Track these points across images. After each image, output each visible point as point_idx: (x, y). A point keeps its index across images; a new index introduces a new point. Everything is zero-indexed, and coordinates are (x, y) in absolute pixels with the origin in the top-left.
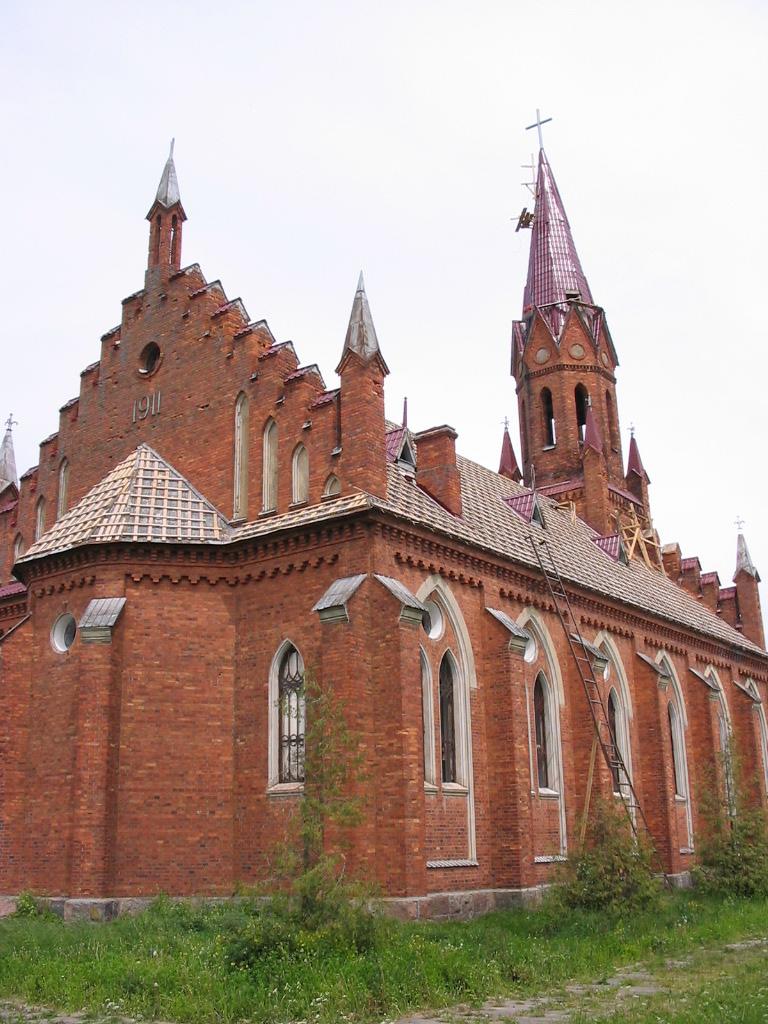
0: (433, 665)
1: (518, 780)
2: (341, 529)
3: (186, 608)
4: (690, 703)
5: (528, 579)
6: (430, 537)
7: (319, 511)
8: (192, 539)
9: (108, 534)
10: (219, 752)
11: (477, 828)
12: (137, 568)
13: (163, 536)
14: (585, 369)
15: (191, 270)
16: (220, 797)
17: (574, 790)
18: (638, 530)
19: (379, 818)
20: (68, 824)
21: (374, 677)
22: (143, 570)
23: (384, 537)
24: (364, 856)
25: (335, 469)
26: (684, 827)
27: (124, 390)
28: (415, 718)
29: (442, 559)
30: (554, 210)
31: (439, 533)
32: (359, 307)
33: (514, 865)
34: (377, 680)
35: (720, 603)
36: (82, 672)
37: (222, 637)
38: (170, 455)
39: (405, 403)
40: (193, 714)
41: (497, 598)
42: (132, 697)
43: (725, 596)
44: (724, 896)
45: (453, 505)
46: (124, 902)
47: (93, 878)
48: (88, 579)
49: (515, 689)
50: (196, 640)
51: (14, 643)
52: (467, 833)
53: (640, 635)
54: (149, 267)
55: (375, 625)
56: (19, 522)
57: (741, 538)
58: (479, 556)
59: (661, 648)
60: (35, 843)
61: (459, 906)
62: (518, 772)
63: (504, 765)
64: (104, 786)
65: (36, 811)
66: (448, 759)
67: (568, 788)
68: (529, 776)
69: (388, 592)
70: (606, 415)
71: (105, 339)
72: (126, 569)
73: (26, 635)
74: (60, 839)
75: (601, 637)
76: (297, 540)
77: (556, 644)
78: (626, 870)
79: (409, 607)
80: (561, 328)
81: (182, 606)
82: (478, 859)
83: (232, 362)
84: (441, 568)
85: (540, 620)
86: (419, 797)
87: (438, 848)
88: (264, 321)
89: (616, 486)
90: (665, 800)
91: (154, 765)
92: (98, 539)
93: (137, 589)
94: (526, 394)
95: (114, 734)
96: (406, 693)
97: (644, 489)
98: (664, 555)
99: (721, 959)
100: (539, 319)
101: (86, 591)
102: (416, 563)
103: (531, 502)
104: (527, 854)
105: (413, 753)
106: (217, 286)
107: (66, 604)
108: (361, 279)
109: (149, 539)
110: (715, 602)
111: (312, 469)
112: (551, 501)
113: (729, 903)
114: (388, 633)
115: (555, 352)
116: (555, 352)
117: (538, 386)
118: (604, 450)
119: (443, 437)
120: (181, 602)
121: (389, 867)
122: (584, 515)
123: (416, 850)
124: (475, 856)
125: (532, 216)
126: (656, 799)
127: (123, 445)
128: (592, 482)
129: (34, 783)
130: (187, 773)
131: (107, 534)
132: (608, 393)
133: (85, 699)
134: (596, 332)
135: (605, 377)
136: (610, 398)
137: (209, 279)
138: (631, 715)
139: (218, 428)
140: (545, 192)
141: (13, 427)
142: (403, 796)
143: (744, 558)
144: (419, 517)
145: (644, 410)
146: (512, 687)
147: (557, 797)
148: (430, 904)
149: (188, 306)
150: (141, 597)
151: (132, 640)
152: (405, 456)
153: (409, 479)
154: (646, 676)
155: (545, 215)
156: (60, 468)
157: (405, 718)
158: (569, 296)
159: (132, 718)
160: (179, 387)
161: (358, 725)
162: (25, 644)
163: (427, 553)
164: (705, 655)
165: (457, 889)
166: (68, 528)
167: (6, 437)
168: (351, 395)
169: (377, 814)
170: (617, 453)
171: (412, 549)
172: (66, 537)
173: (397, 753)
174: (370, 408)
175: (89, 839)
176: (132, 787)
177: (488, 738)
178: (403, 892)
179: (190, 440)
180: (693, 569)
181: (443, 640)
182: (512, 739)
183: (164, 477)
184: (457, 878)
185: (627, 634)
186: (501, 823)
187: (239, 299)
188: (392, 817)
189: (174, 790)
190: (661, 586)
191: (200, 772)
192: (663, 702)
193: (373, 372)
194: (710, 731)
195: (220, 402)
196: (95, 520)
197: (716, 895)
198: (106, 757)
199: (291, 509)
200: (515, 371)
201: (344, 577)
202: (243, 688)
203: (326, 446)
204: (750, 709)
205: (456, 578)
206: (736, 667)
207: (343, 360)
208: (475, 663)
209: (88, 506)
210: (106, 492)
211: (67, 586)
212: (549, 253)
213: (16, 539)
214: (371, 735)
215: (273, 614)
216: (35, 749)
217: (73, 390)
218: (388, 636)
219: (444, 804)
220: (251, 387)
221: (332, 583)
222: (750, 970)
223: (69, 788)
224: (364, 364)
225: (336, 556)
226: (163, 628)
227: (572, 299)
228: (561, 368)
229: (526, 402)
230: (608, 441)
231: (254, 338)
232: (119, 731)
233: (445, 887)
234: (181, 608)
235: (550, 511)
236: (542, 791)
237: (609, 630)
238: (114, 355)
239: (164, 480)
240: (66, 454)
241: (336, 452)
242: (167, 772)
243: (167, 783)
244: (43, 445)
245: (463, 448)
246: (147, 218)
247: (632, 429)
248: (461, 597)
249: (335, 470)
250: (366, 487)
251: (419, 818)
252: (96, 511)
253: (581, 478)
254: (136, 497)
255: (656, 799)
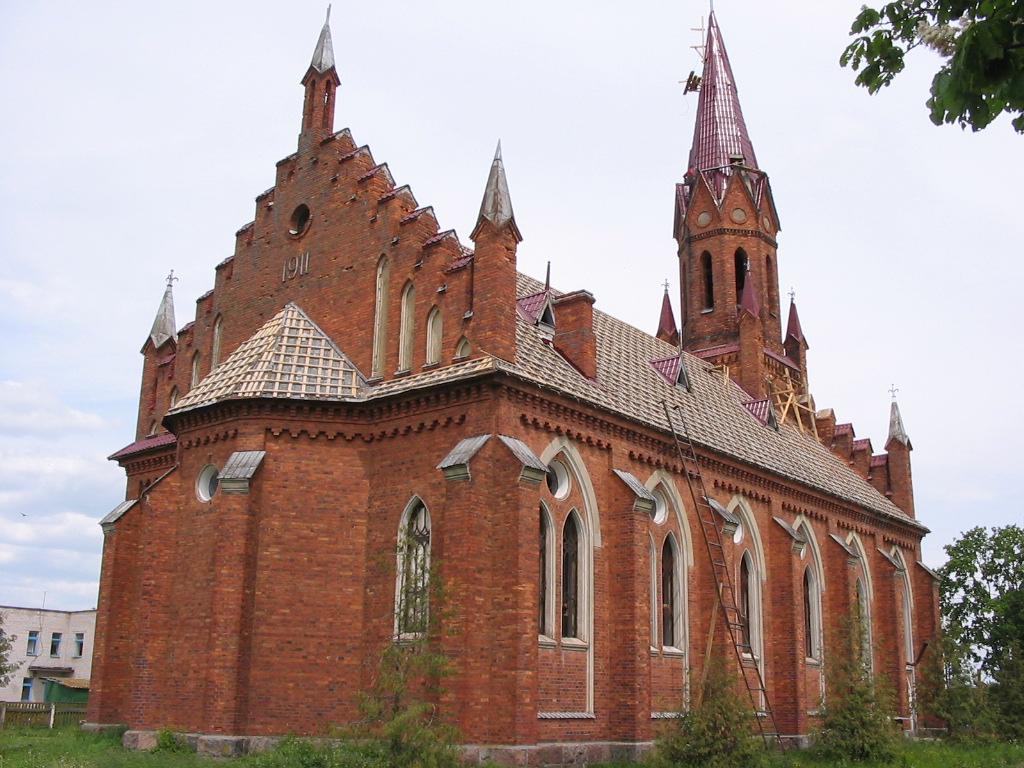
0: (557, 524)
1: (637, 637)
2: (468, 391)
3: (323, 462)
4: (829, 568)
6: (557, 401)
7: (433, 377)
8: (330, 396)
9: (249, 390)
10: (349, 600)
12: (276, 423)
13: (303, 392)
14: (745, 233)
15: (341, 135)
16: (349, 645)
18: (791, 395)
19: (493, 669)
20: (206, 665)
21: (494, 534)
22: (282, 425)
24: (477, 704)
25: (466, 332)
27: (276, 250)
28: (531, 575)
30: (722, 75)
32: (496, 175)
33: (630, 719)
35: (871, 470)
36: (222, 521)
37: (357, 491)
38: (315, 314)
40: (325, 564)
41: (626, 460)
42: (269, 546)
43: (877, 463)
45: (588, 369)
46: (258, 742)
47: (225, 716)
48: (231, 433)
50: (331, 493)
51: (161, 492)
52: (585, 687)
53: (777, 500)
54: (302, 130)
55: (497, 483)
56: (176, 376)
57: (894, 406)
60: (176, 682)
63: (624, 623)
64: (238, 629)
65: (177, 651)
67: (694, 646)
69: (510, 452)
70: (765, 279)
71: (259, 200)
72: (266, 423)
73: (173, 484)
74: (198, 679)
75: (735, 501)
76: (427, 400)
77: (687, 506)
79: (528, 468)
80: (724, 192)
81: (318, 460)
83: (376, 226)
84: (569, 431)
85: (671, 483)
87: (555, 700)
88: (408, 186)
89: (773, 351)
90: (794, 662)
91: (287, 611)
92: (240, 395)
93: (277, 443)
95: (250, 581)
96: (523, 550)
100: (702, 182)
101: (229, 443)
102: (541, 425)
104: (643, 709)
105: (528, 608)
106: (366, 151)
107: (210, 456)
108: (499, 148)
109: (288, 395)
110: (867, 468)
112: (707, 365)
114: (509, 492)
115: (716, 216)
116: (716, 216)
117: (698, 249)
118: (761, 315)
120: (317, 457)
121: (501, 716)
122: (739, 379)
123: (528, 700)
124: (592, 710)
125: (700, 79)
126: (785, 660)
127: (273, 303)
129: (176, 625)
130: (318, 620)
131: (249, 390)
132: (768, 257)
133: (224, 547)
134: (758, 198)
135: (766, 242)
136: (770, 264)
137: (359, 144)
139: (360, 289)
140: (714, 54)
141: (174, 283)
142: (516, 649)
143: (897, 427)
144: (547, 380)
145: (807, 275)
147: (681, 656)
148: (539, 753)
149: (337, 170)
150: (281, 451)
151: (270, 493)
153: (546, 342)
154: (781, 541)
155: (713, 79)
156: (215, 324)
158: (732, 160)
159: (268, 566)
160: (326, 249)
161: (476, 579)
162: (172, 493)
165: (572, 740)
166: (214, 383)
167: (166, 293)
168: (485, 261)
170: (776, 318)
172: (212, 391)
174: (501, 273)
175: (224, 680)
176: (266, 631)
178: (512, 740)
179: (335, 300)
180: (846, 435)
182: (633, 598)
183: (308, 336)
184: (572, 729)
185: (763, 499)
187: (385, 164)
188: (505, 669)
189: (306, 636)
191: (330, 619)
192: (798, 569)
195: (363, 264)
196: (239, 376)
198: (240, 602)
199: (424, 370)
202: (374, 540)
204: (892, 576)
205: (584, 440)
207: (477, 226)
209: (235, 362)
210: (253, 349)
211: (212, 439)
212: (714, 117)
213: (172, 392)
215: (404, 470)
216: (178, 594)
217: (228, 249)
218: (508, 495)
220: (392, 251)
221: (459, 441)
223: (207, 631)
224: (498, 230)
226: (302, 483)
228: (722, 232)
229: (687, 264)
230: (766, 306)
231: (396, 203)
232: (254, 578)
233: (560, 737)
234: (316, 462)
235: (703, 374)
236: (666, 649)
237: (744, 494)
238: (267, 216)
239: (307, 339)
240: (220, 310)
242: (300, 618)
243: (300, 629)
244: (200, 301)
246: (302, 82)
248: (588, 458)
250: (494, 351)
251: (532, 670)
252: (242, 367)
253: (738, 342)
254: (328, 360)
255: (785, 660)
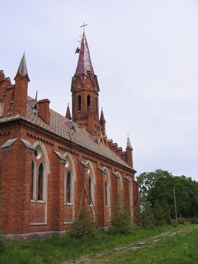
0: (37, 166)
1: (60, 200)
2: (11, 125)
5: (67, 144)
6: (38, 129)
7: (6, 119)
11: (48, 214)
14: (90, 91)
17: (78, 204)
23: (24, 128)
24: (11, 221)
26: (108, 214)
29: (42, 136)
31: (41, 128)
32: (23, 62)
33: (58, 224)
34: (18, 169)
35: (122, 155)
39: (37, 92)
43: (123, 154)
44: (117, 234)
45: (47, 122)
49: (61, 174)
52: (44, 215)
53: (99, 162)
57: (128, 139)
58: (53, 136)
59: (105, 166)
61: (41, 236)
62: (60, 198)
63: (57, 196)
66: (40, 194)
67: (76, 203)
68: (64, 199)
69: (23, 144)
75: (88, 162)
77: (75, 163)
78: (88, 227)
79: (29, 148)
80: (85, 80)
82: (47, 223)
85: (70, 156)
86: (29, 204)
87: (35, 219)
89: (97, 123)
90: (103, 207)
94: (74, 97)
96: (27, 173)
97: (104, 124)
98: (108, 142)
99: (111, 254)
100: (79, 77)
102: (33, 136)
103: (72, 124)
105: (28, 191)
108: (24, 54)
110: (121, 155)
111: (5, 107)
113: (119, 235)
114: (23, 155)
116: (82, 85)
117: (78, 95)
119: (46, 102)
121: (19, 225)
122: (87, 130)
124: (46, 222)
125: (80, 49)
126: (101, 206)
128: (90, 121)
134: (94, 81)
136: (97, 100)
138: (95, 184)
140: (84, 44)
143: (129, 144)
145: (106, 104)
146: (60, 174)
148: (30, 236)
152: (35, 107)
153: (35, 113)
154: (100, 173)
155: (83, 50)
157: (26, 181)
158: (88, 71)
161: (11, 182)
163: (37, 134)
164: (117, 168)
165: (40, 231)
168: (18, 86)
169: (16, 209)
170: (98, 114)
171: (32, 132)
173: (23, 191)
177: (52, 188)
178: (22, 232)
180: (115, 146)
181: (41, 159)
182: (59, 188)
186: (55, 212)
190: (106, 150)
192: (104, 181)
193: (25, 80)
194: (117, 189)
197: (114, 233)
200: (72, 90)
201: (11, 139)
203: (9, 100)
206: (125, 172)
208: (50, 167)
212: (83, 60)
214: (16, 185)
218: (22, 157)
219: (38, 207)
222: (119, 258)
224: (22, 78)
225: (9, 133)
227: (88, 72)
228: (84, 90)
230: (95, 111)
233: (37, 230)
235: (78, 128)
236: (68, 204)
241: (12, 102)
245: (52, 106)
247: (102, 108)
249: (11, 107)
250: (20, 113)
251: (29, 210)
255: (101, 206)
